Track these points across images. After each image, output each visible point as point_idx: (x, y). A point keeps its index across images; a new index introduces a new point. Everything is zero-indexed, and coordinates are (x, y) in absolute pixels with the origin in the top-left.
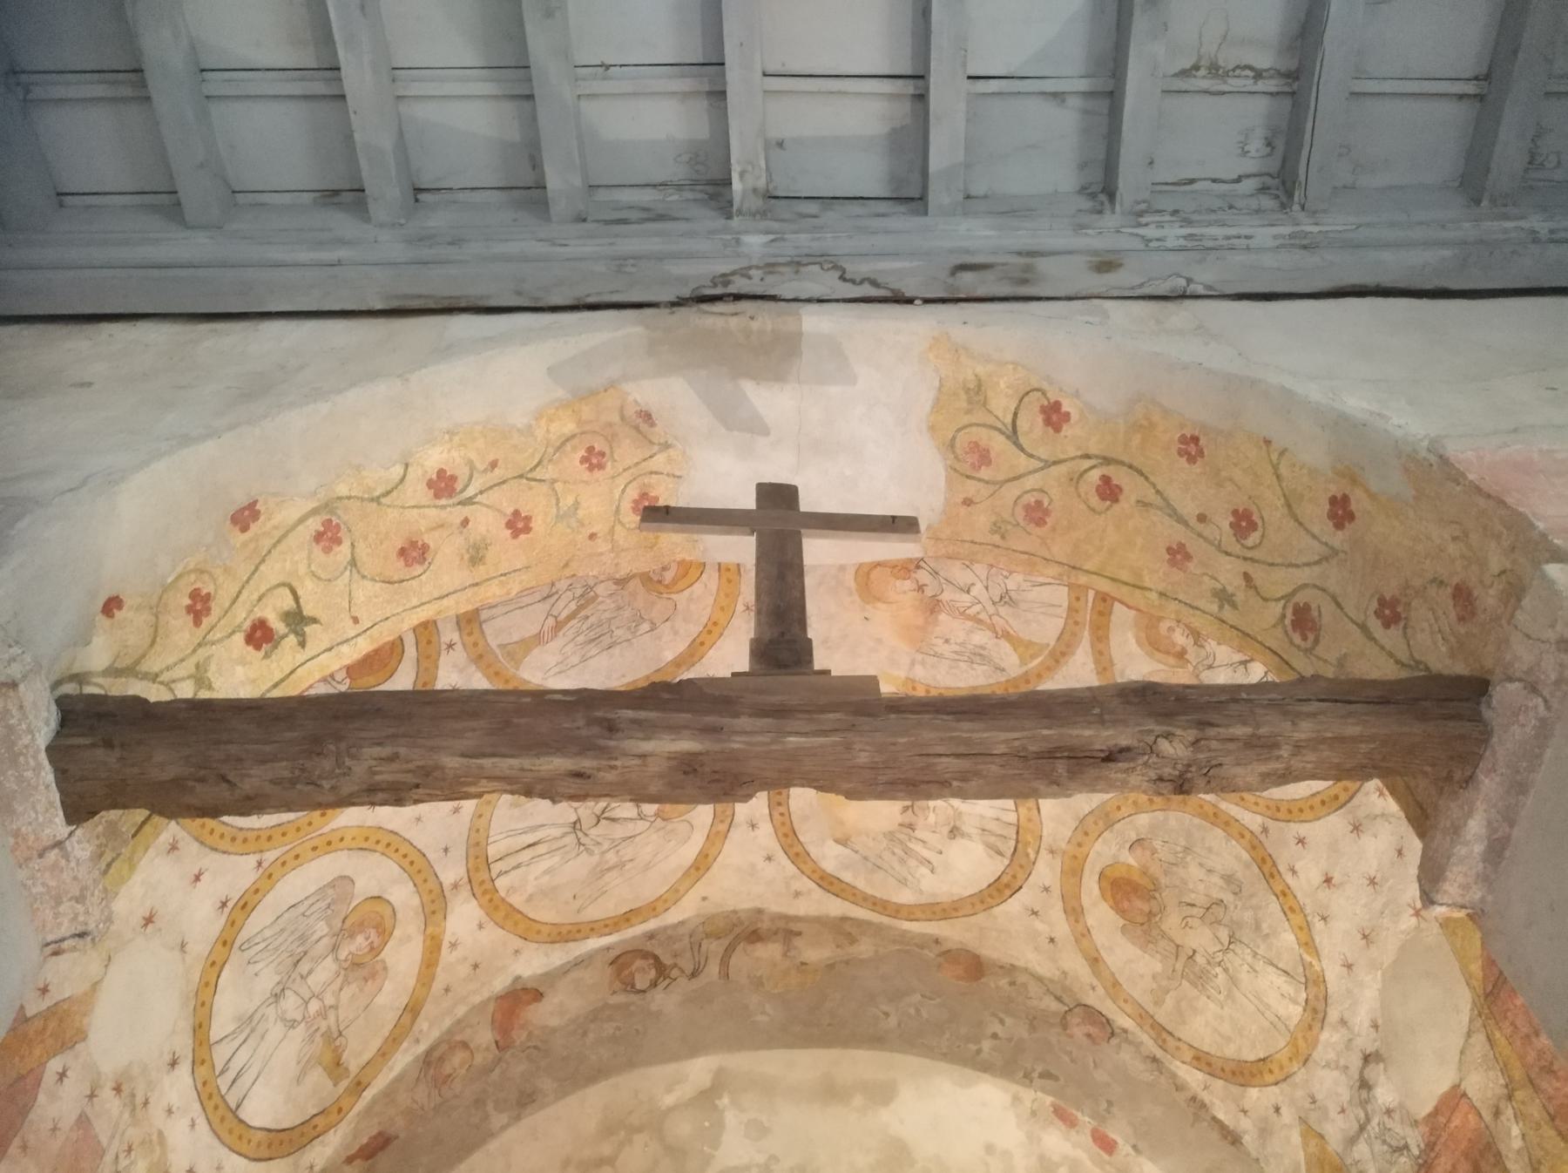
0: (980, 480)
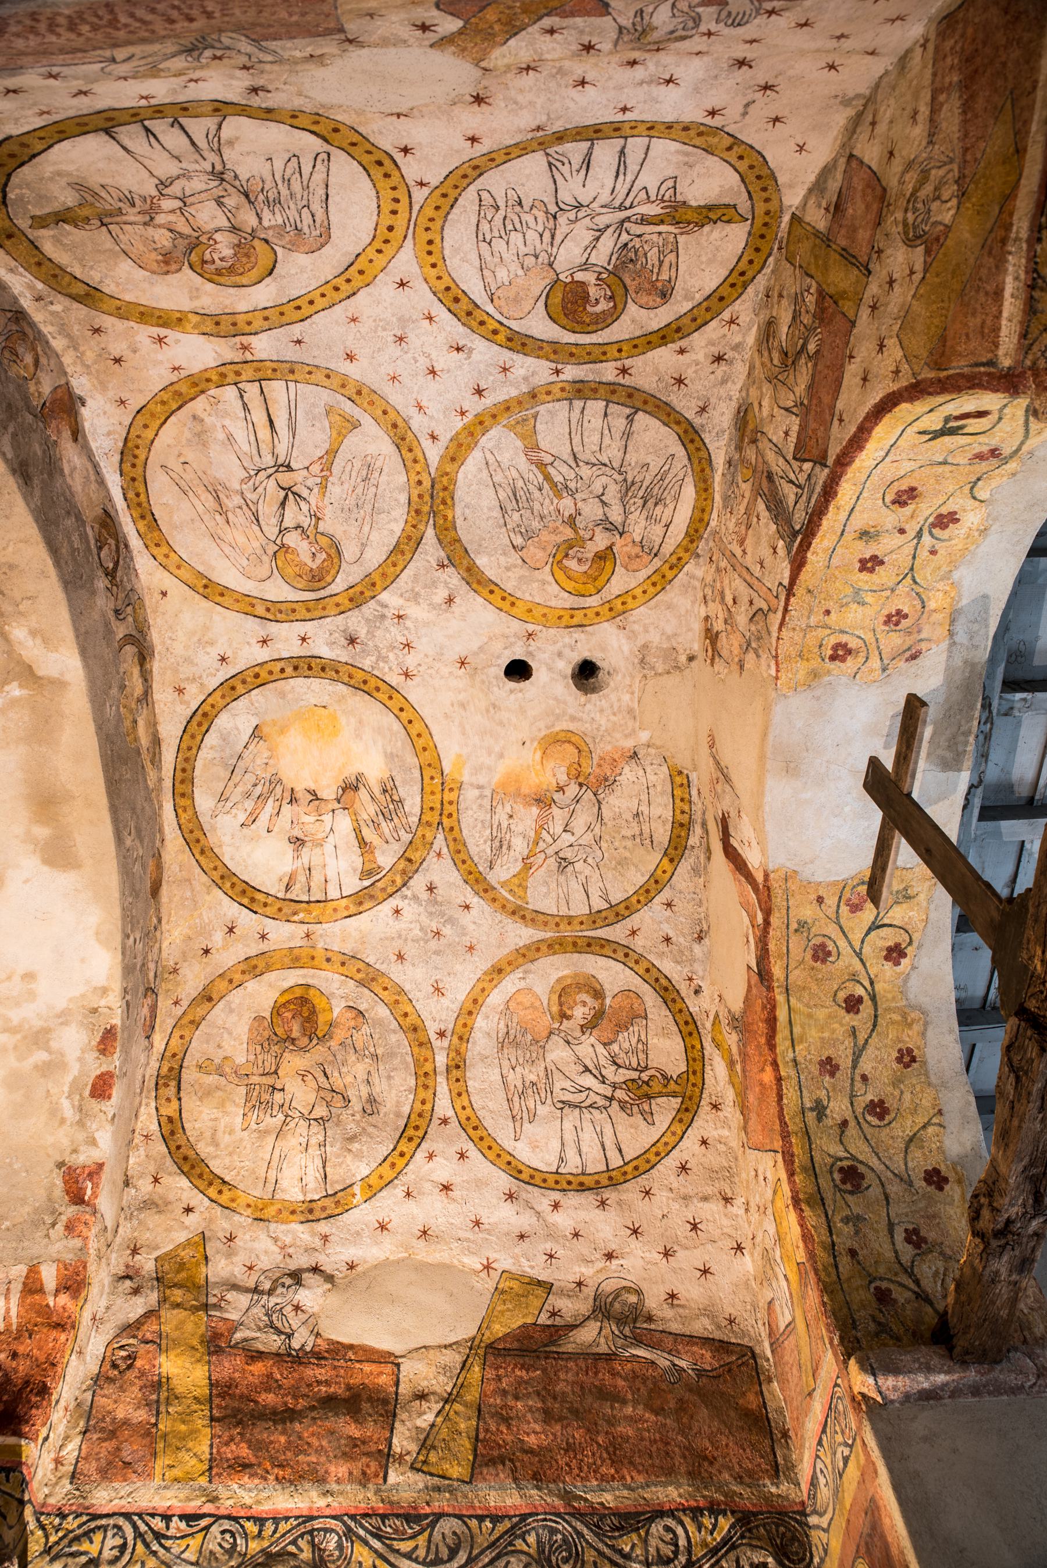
0: (838, 906)
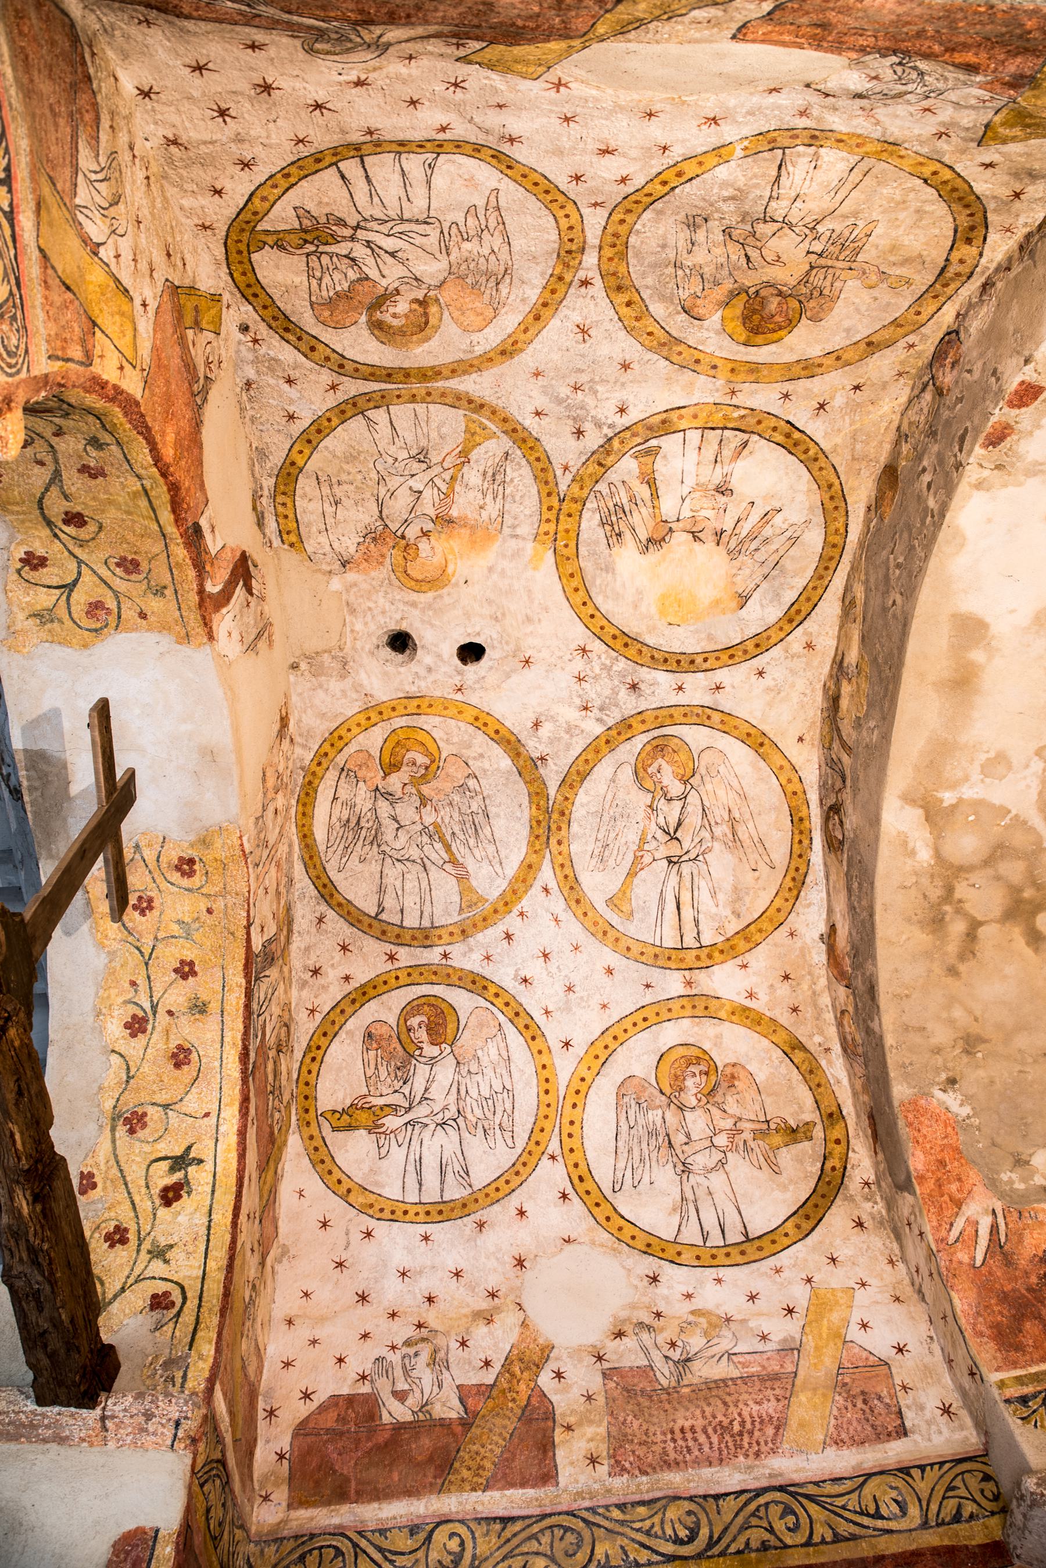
0: (119, 608)
